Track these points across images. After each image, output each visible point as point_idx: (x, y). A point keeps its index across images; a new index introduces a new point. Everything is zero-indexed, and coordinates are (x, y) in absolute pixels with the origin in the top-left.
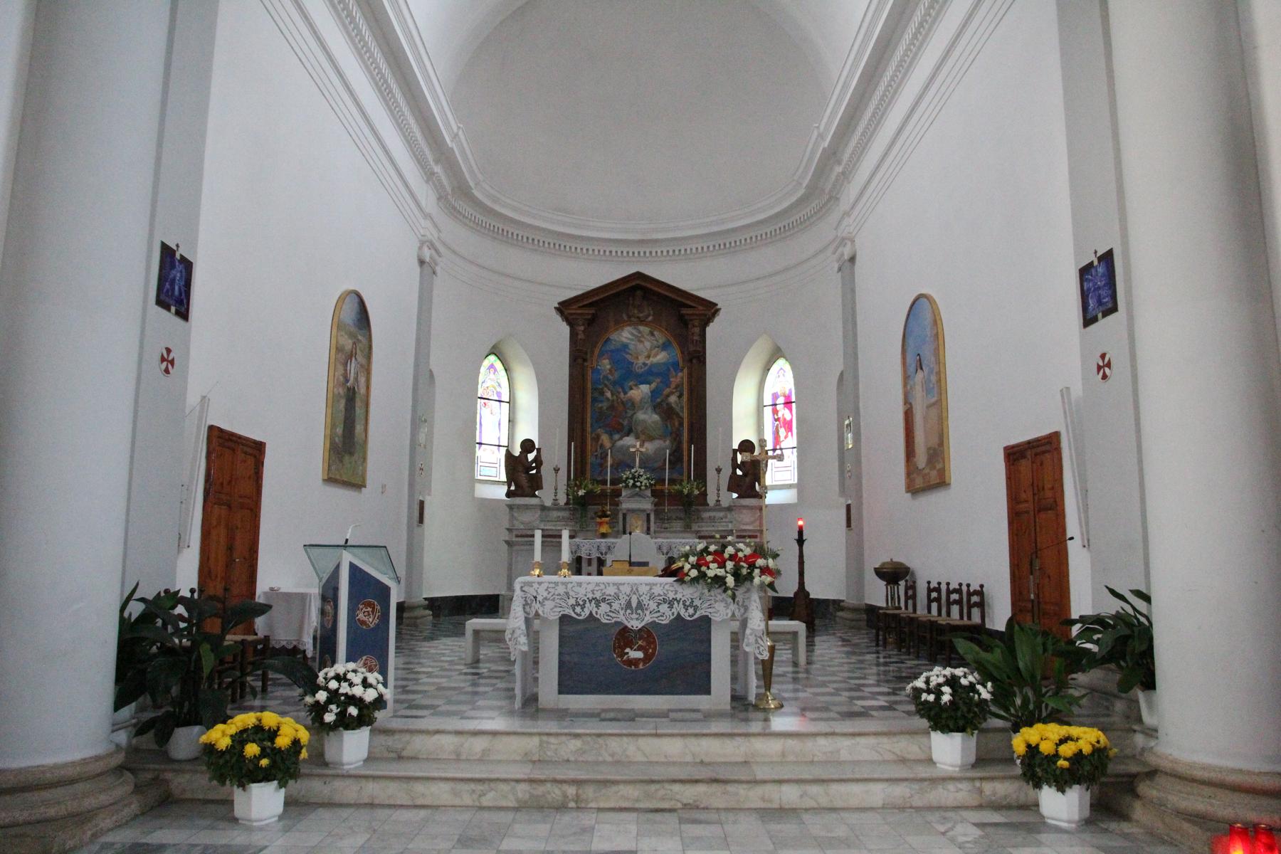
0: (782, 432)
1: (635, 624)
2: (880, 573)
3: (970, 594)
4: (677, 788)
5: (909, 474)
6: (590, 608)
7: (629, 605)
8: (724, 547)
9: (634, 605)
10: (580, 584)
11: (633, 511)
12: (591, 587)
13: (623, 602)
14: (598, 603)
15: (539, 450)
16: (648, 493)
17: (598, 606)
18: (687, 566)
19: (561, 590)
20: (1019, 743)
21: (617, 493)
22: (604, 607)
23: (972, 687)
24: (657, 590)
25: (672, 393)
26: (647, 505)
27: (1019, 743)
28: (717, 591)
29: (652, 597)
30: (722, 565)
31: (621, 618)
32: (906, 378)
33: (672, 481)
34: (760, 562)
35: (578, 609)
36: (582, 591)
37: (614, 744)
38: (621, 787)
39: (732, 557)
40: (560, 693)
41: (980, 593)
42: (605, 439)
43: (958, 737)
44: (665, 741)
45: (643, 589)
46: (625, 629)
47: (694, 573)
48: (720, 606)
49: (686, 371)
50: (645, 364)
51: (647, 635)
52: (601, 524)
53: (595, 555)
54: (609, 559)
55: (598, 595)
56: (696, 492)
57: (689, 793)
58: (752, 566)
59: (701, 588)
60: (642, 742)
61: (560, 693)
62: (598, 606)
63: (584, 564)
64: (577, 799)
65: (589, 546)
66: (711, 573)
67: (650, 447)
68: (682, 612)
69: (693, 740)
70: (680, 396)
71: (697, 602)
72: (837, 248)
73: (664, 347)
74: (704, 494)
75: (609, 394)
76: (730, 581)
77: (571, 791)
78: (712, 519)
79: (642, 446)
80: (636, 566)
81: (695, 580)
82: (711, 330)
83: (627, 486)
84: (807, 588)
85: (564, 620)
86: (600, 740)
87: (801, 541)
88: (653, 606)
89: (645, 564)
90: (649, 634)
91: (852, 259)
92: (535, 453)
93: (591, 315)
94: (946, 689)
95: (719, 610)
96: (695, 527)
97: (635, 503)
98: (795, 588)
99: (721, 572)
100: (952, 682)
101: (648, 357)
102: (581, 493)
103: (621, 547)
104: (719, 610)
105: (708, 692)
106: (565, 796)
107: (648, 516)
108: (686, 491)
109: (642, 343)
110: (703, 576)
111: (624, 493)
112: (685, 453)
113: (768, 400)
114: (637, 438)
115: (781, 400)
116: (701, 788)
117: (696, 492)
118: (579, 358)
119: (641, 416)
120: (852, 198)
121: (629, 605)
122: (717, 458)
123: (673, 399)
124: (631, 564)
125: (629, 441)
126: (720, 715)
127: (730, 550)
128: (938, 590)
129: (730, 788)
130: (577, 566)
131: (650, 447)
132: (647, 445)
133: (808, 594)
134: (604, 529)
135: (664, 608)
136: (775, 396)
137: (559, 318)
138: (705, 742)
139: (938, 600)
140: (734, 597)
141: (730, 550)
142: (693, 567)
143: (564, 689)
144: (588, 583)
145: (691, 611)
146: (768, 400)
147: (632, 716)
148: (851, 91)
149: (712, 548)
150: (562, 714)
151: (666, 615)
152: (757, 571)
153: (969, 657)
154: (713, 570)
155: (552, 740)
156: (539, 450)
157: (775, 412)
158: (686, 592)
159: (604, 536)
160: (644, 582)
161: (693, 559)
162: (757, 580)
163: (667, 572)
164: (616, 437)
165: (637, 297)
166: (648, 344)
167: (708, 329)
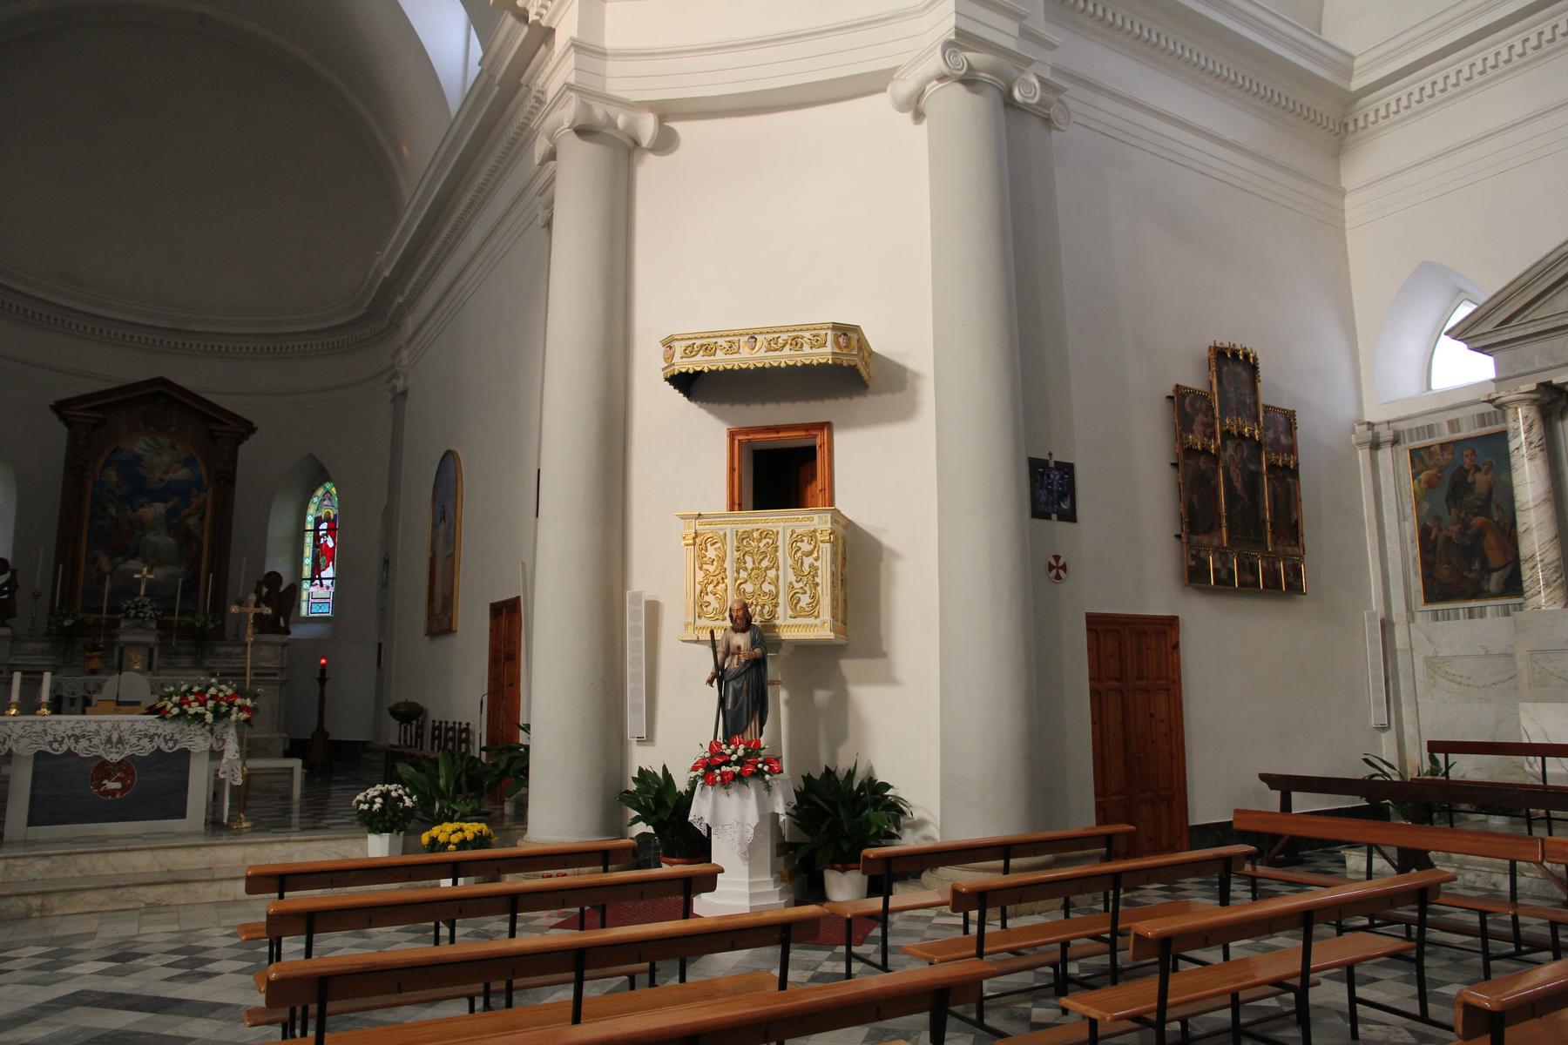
0: (322, 560)
1: (114, 757)
2: (394, 712)
3: (447, 730)
4: (141, 890)
5: (429, 618)
6: (69, 744)
7: (109, 740)
8: (208, 687)
9: (115, 739)
10: (59, 722)
11: (133, 644)
12: (70, 725)
13: (104, 738)
14: (77, 739)
15: (14, 572)
16: (154, 625)
17: (77, 741)
18: (170, 705)
19: (39, 727)
20: (425, 838)
21: (115, 624)
22: (84, 743)
23: (400, 798)
24: (138, 726)
25: (190, 515)
26: (151, 639)
27: (425, 838)
28: (195, 727)
29: (132, 733)
30: (203, 704)
31: (101, 752)
32: (434, 526)
33: (182, 612)
34: (239, 701)
35: (56, 745)
36: (60, 729)
37: (84, 861)
38: (88, 893)
39: (213, 697)
40: (30, 824)
41: (467, 730)
42: (105, 563)
43: (386, 836)
44: (135, 854)
45: (124, 726)
46: (105, 762)
47: (176, 711)
48: (199, 740)
49: (210, 491)
50: (161, 480)
51: (126, 767)
52: (90, 658)
53: (81, 693)
54: (95, 698)
55: (78, 732)
56: (211, 626)
57: (152, 894)
58: (231, 705)
59: (181, 724)
60: (111, 857)
61: (30, 824)
62: (77, 741)
63: (65, 704)
64: (42, 908)
65: (75, 683)
66: (191, 711)
67: (160, 573)
68: (163, 746)
69: (161, 852)
70: (202, 519)
71: (177, 736)
72: (389, 381)
73: (189, 462)
74: (222, 627)
75: (113, 511)
76: (209, 717)
77: (36, 902)
78: (228, 655)
79: (149, 572)
80: (121, 705)
81: (177, 717)
82: (243, 449)
83: (127, 617)
84: (327, 727)
85: (40, 756)
86: (70, 859)
87: (322, 680)
88: (133, 740)
89: (137, 703)
90: (128, 766)
91: (404, 393)
92: (8, 575)
93: (93, 419)
94: (379, 800)
95: (198, 742)
96: (207, 663)
97: (136, 635)
98: (314, 728)
99: (201, 710)
100: (385, 795)
101: (166, 472)
102: (67, 623)
103: (112, 685)
104: (198, 742)
105: (183, 815)
106: (29, 907)
107: (151, 650)
108: (198, 625)
109: (162, 457)
110: (183, 713)
111: (123, 624)
112: (202, 583)
113: (310, 526)
114: (145, 562)
115: (324, 526)
116: (164, 889)
117: (211, 626)
118: (76, 467)
119: (152, 538)
120: (410, 331)
121: (109, 740)
122: (241, 576)
123: (192, 521)
124: (119, 703)
125: (133, 564)
126: (193, 834)
127: (213, 691)
128: (439, 728)
129: (191, 887)
130: (57, 706)
131: (160, 573)
132: (156, 570)
133: (327, 735)
134: (95, 664)
135: (145, 742)
136: (318, 521)
137: (54, 417)
138: (172, 854)
139: (439, 738)
140: (212, 731)
141: (213, 691)
142: (175, 705)
143: (32, 822)
144: (68, 722)
145: (171, 744)
146: (310, 526)
147: (104, 839)
148: (457, 156)
149: (196, 689)
150: (26, 843)
151: (147, 748)
152: (235, 709)
153: (405, 776)
154: (195, 708)
155: (20, 862)
156: (14, 572)
157: (317, 538)
158: (168, 728)
159: (93, 672)
160: (125, 720)
161: (176, 699)
162: (233, 717)
163: (152, 710)
164: (119, 559)
165: (158, 401)
166: (167, 458)
167: (242, 449)
